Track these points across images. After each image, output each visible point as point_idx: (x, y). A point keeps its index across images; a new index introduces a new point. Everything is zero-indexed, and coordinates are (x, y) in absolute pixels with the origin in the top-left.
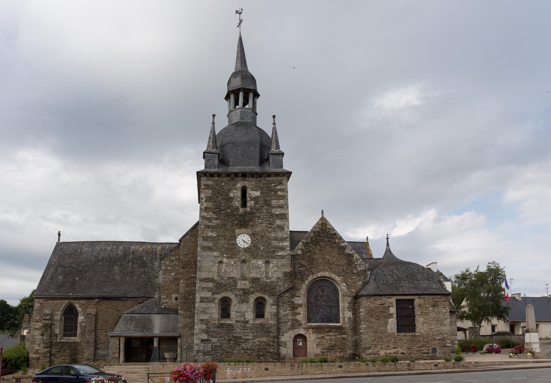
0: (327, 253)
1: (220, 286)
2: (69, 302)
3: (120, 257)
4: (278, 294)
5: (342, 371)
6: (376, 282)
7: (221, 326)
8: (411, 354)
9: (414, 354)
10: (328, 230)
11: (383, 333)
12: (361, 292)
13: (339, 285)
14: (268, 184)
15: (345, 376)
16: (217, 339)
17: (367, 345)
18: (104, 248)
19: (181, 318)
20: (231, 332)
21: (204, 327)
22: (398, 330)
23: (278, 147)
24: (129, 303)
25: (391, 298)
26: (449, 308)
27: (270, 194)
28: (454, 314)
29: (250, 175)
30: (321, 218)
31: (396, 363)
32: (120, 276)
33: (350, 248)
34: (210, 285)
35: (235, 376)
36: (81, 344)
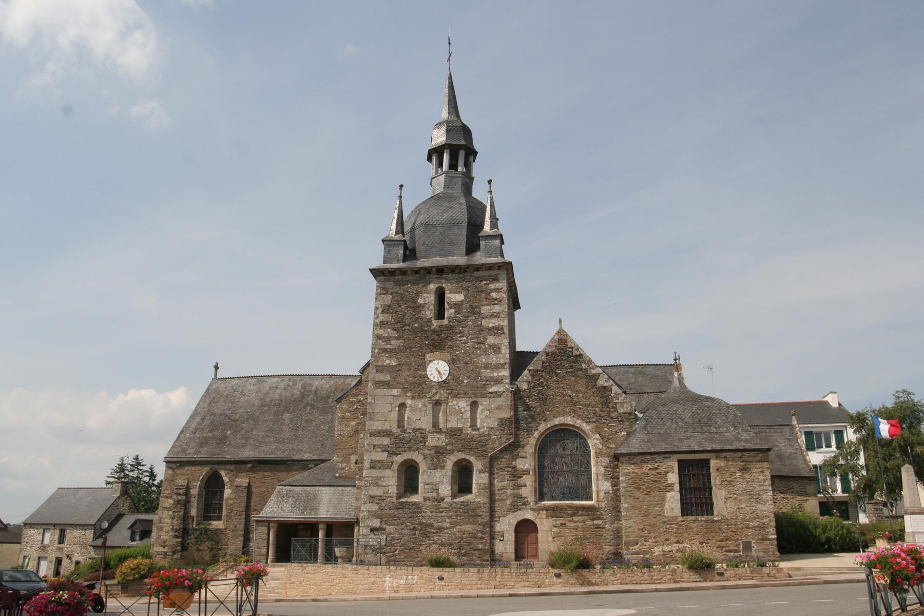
0: (568, 387)
1: (401, 443)
2: (212, 467)
10: (570, 350)
17: (631, 538)
21: (375, 507)
23: (494, 225)
25: (670, 457)
26: (770, 473)
27: (479, 297)
28: (812, 480)
34: (386, 441)
35: (396, 589)
36: (226, 532)
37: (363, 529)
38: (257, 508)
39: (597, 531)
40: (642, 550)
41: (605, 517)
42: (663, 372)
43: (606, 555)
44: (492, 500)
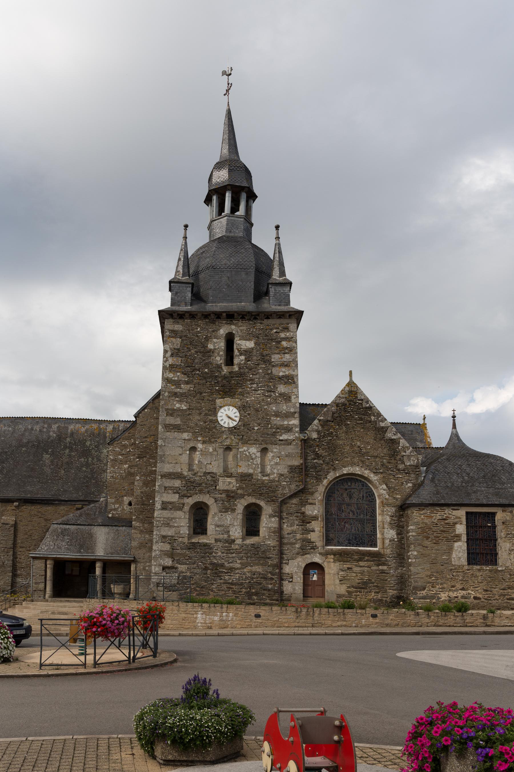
1: (192, 486)
3: (52, 440)
4: (280, 500)
5: (377, 623)
6: (434, 485)
7: (193, 546)
8: (490, 600)
9: (494, 600)
11: (445, 565)
12: (410, 499)
13: (376, 488)
14: (267, 329)
15: (379, 632)
16: (186, 566)
17: (420, 584)
18: (30, 427)
19: (136, 533)
20: (208, 557)
21: (167, 547)
22: (470, 561)
23: (282, 273)
24: (62, 508)
25: (459, 510)
29: (239, 315)
30: (349, 382)
31: (464, 614)
32: (51, 469)
33: (394, 429)
34: (177, 483)
35: (209, 625)
37: (155, 568)
38: (24, 546)
39: (382, 576)
40: (430, 595)
41: (390, 564)
42: (409, 431)
43: (390, 599)
44: (281, 544)
